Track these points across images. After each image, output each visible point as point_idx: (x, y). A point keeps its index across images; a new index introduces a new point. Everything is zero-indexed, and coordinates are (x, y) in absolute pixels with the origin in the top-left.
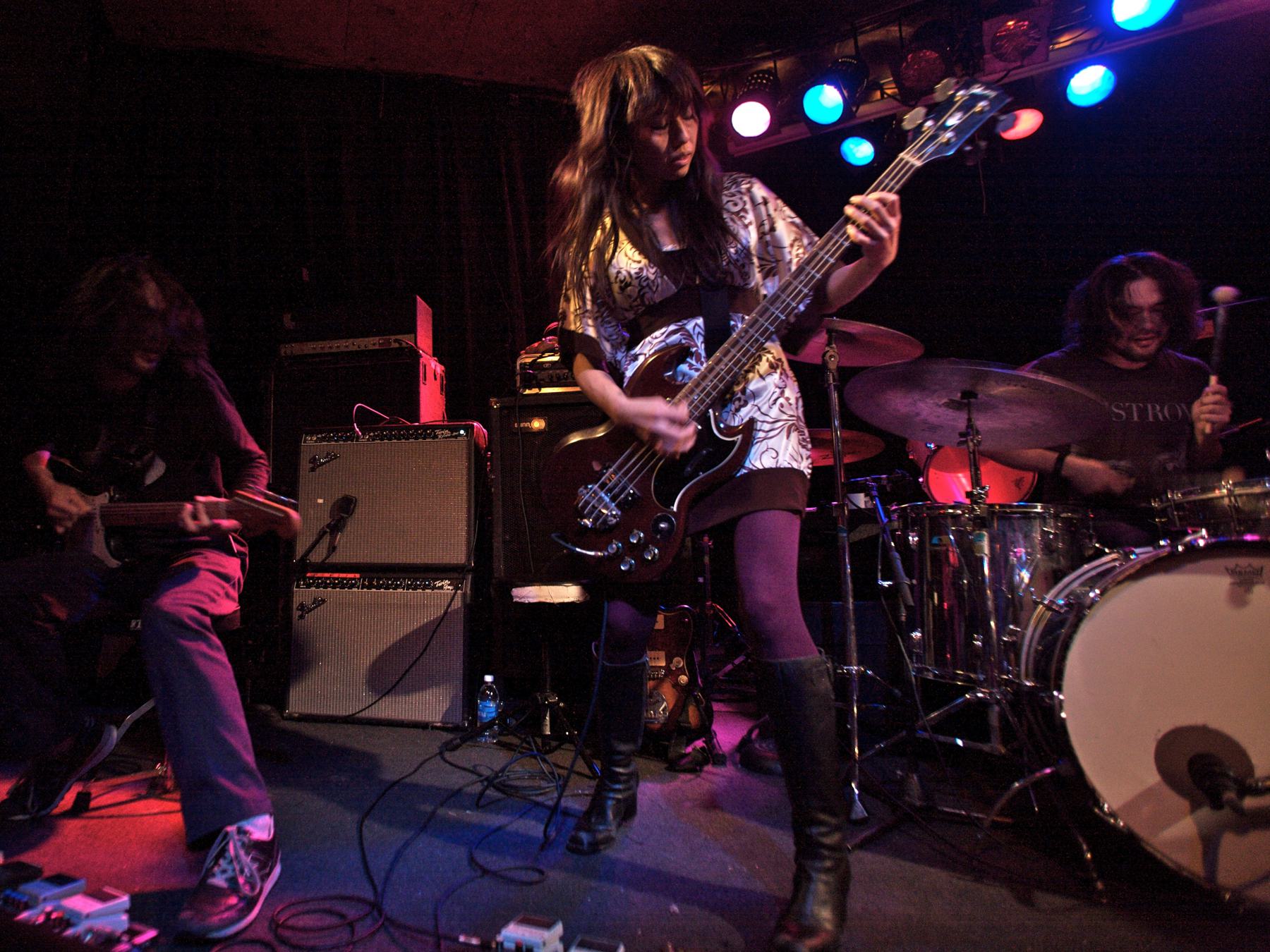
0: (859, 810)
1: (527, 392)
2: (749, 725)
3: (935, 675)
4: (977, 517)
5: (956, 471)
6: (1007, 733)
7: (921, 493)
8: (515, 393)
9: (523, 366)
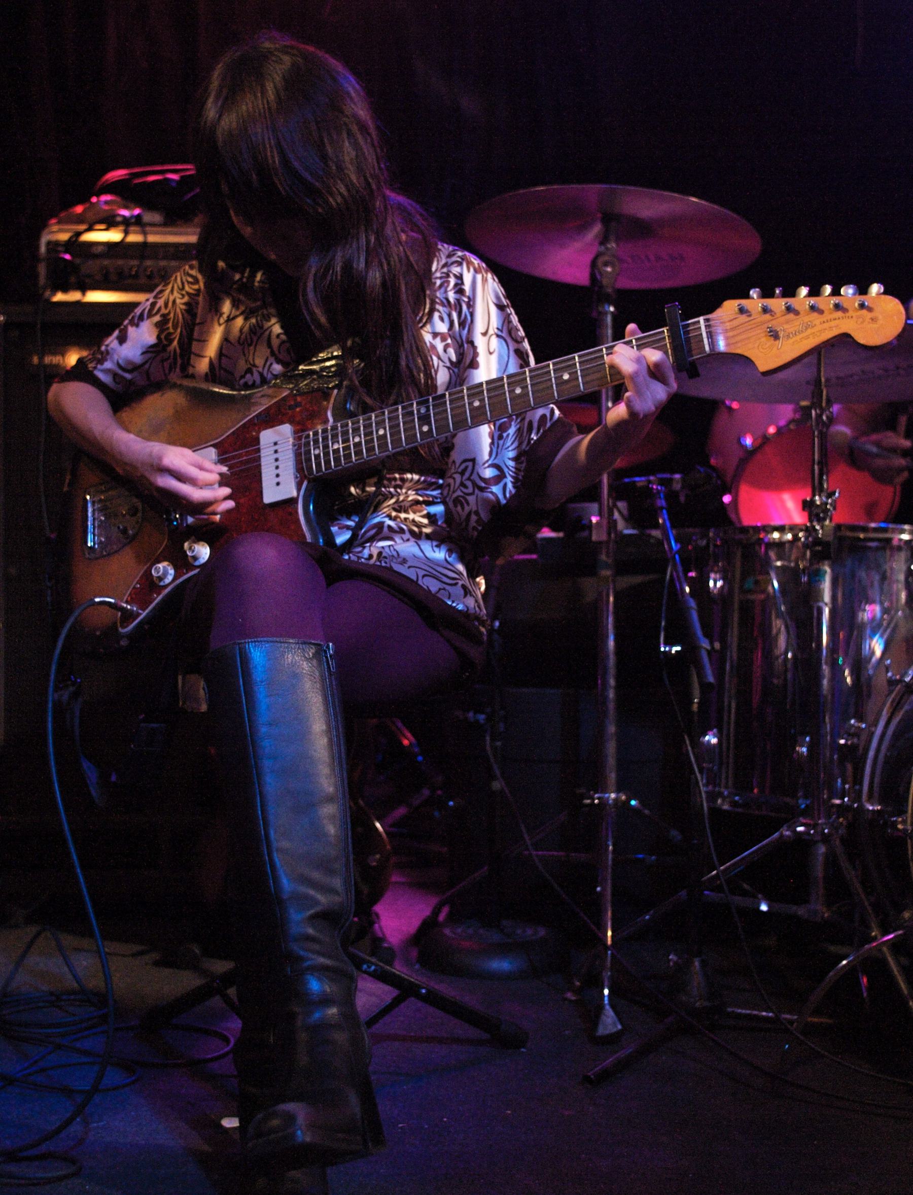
0: (609, 1023)
1: (59, 297)
2: (434, 901)
3: (734, 804)
4: (818, 542)
5: (779, 488)
6: (837, 889)
7: (722, 517)
8: (36, 298)
9: (53, 246)
